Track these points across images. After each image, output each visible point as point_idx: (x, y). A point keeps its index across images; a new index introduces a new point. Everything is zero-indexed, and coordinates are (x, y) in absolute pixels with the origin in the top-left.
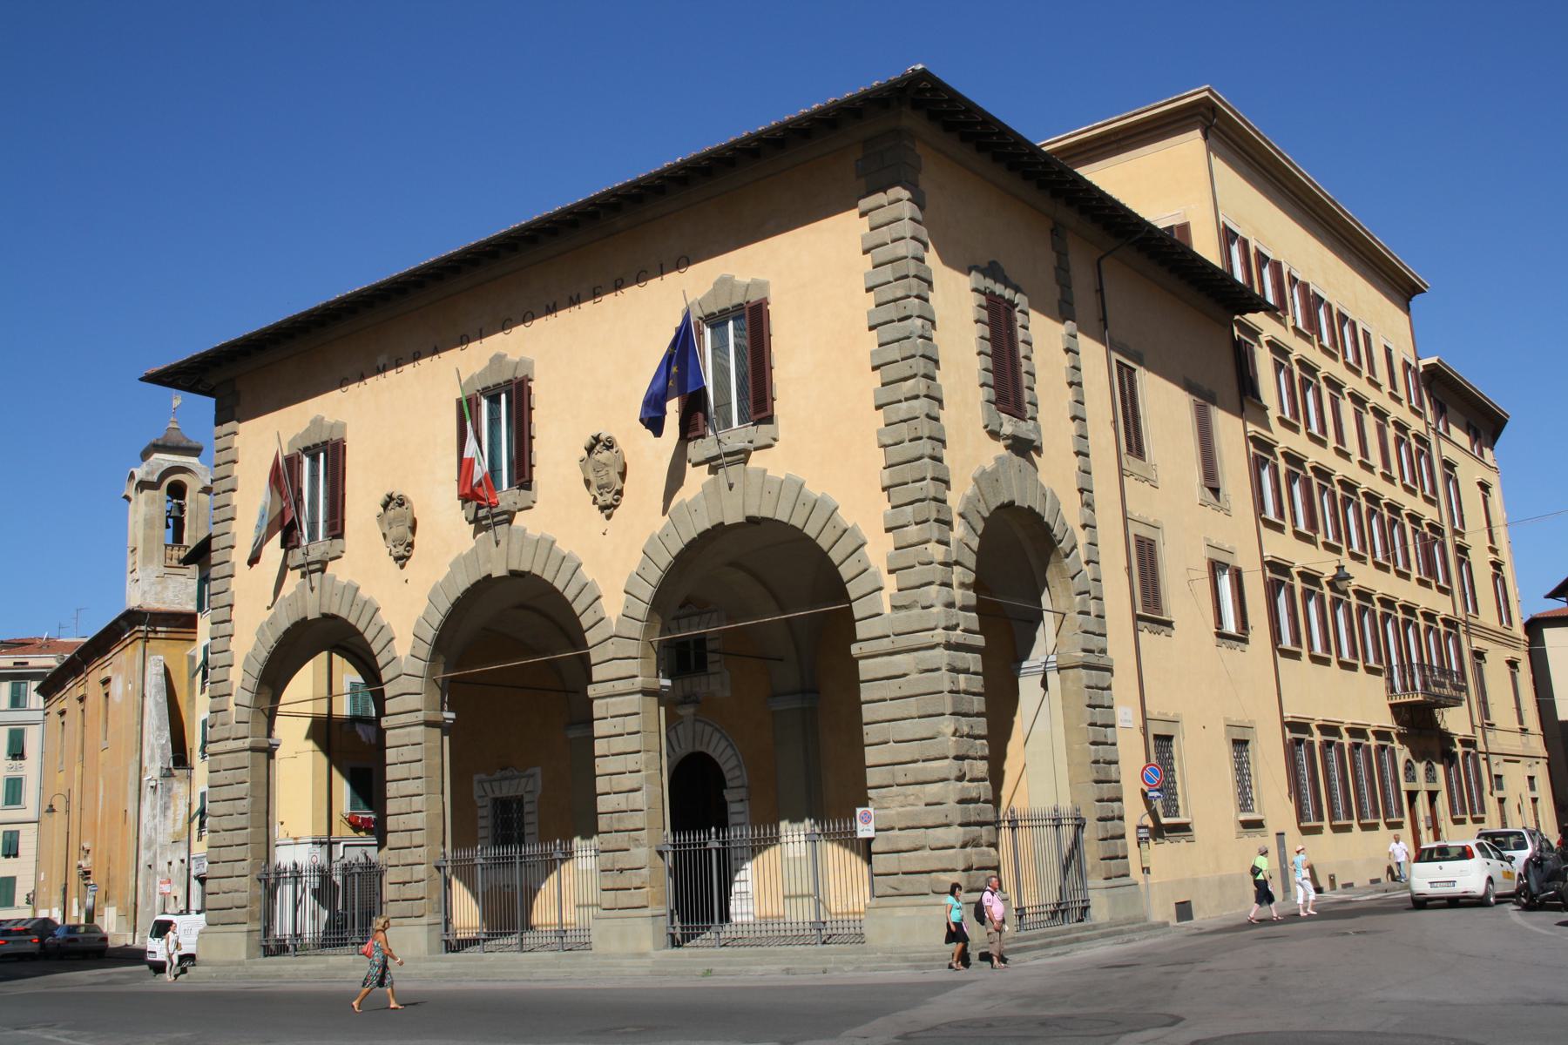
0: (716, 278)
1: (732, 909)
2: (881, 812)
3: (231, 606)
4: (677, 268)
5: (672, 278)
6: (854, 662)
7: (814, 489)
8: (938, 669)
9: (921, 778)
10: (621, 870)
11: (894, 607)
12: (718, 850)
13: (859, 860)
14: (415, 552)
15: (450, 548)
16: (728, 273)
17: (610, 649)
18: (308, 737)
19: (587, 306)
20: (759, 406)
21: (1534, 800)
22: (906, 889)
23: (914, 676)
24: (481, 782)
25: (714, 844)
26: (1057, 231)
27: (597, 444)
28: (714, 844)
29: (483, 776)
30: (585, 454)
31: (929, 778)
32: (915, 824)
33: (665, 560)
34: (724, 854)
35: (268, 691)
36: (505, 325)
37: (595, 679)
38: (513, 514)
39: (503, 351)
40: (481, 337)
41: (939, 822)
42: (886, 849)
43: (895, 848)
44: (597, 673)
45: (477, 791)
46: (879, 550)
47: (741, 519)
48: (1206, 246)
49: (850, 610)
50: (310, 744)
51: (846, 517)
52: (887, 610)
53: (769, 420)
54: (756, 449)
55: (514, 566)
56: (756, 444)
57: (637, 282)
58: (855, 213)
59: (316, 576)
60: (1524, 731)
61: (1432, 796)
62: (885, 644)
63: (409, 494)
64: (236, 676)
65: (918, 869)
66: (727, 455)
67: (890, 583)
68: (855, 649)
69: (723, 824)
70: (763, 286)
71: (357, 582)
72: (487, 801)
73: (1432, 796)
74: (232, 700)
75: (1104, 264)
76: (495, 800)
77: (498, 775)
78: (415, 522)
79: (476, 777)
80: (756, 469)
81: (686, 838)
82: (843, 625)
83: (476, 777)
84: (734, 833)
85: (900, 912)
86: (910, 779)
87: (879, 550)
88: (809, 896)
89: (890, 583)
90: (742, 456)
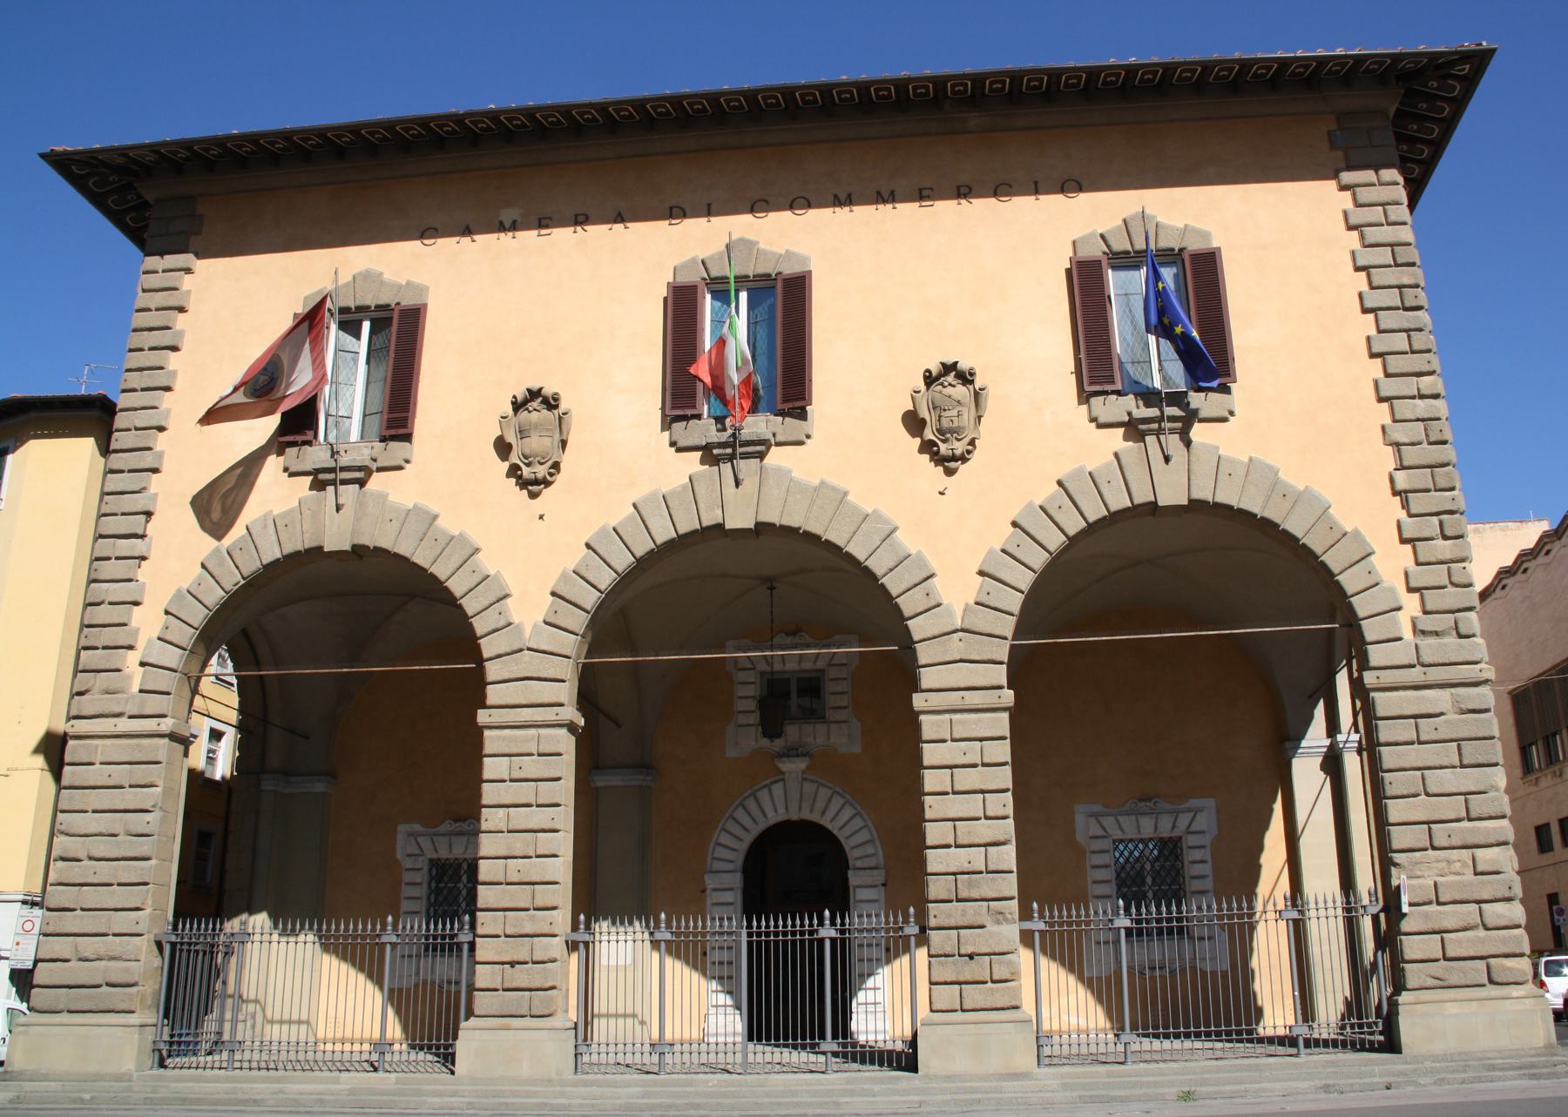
1: (854, 1026)
2: (1414, 882)
3: (149, 514)
4: (1062, 190)
5: (1052, 203)
6: (479, 731)
8: (1487, 710)
9: (1471, 840)
10: (971, 957)
12: (833, 940)
13: (362, 977)
14: (560, 480)
16: (377, 267)
18: (37, 751)
19: (907, 209)
22: (1454, 979)
23: (1452, 716)
24: (410, 834)
25: (827, 932)
27: (535, 398)
28: (827, 932)
29: (417, 827)
30: (509, 410)
31: (1482, 841)
32: (1465, 897)
33: (1295, 526)
34: (841, 947)
35: (201, 650)
36: (757, 205)
37: (489, 701)
38: (368, 471)
40: (1036, 192)
41: (1499, 895)
42: (1423, 928)
43: (1437, 927)
44: (494, 694)
45: (1084, 825)
47: (347, 547)
49: (480, 670)
50: (40, 761)
53: (801, 414)
54: (380, 470)
55: (766, 517)
56: (380, 464)
57: (995, 194)
58: (1331, 185)
59: (349, 493)
62: (953, 699)
64: (147, 623)
65: (1472, 954)
66: (343, 469)
67: (1411, 604)
68: (483, 716)
69: (840, 903)
70: (423, 290)
71: (434, 507)
72: (422, 863)
74: (133, 658)
76: (433, 863)
77: (447, 826)
79: (403, 828)
80: (778, 470)
81: (777, 926)
82: (473, 688)
83: (403, 828)
84: (854, 921)
85: (1452, 1009)
86: (1455, 841)
88: (599, 1016)
90: (760, 446)
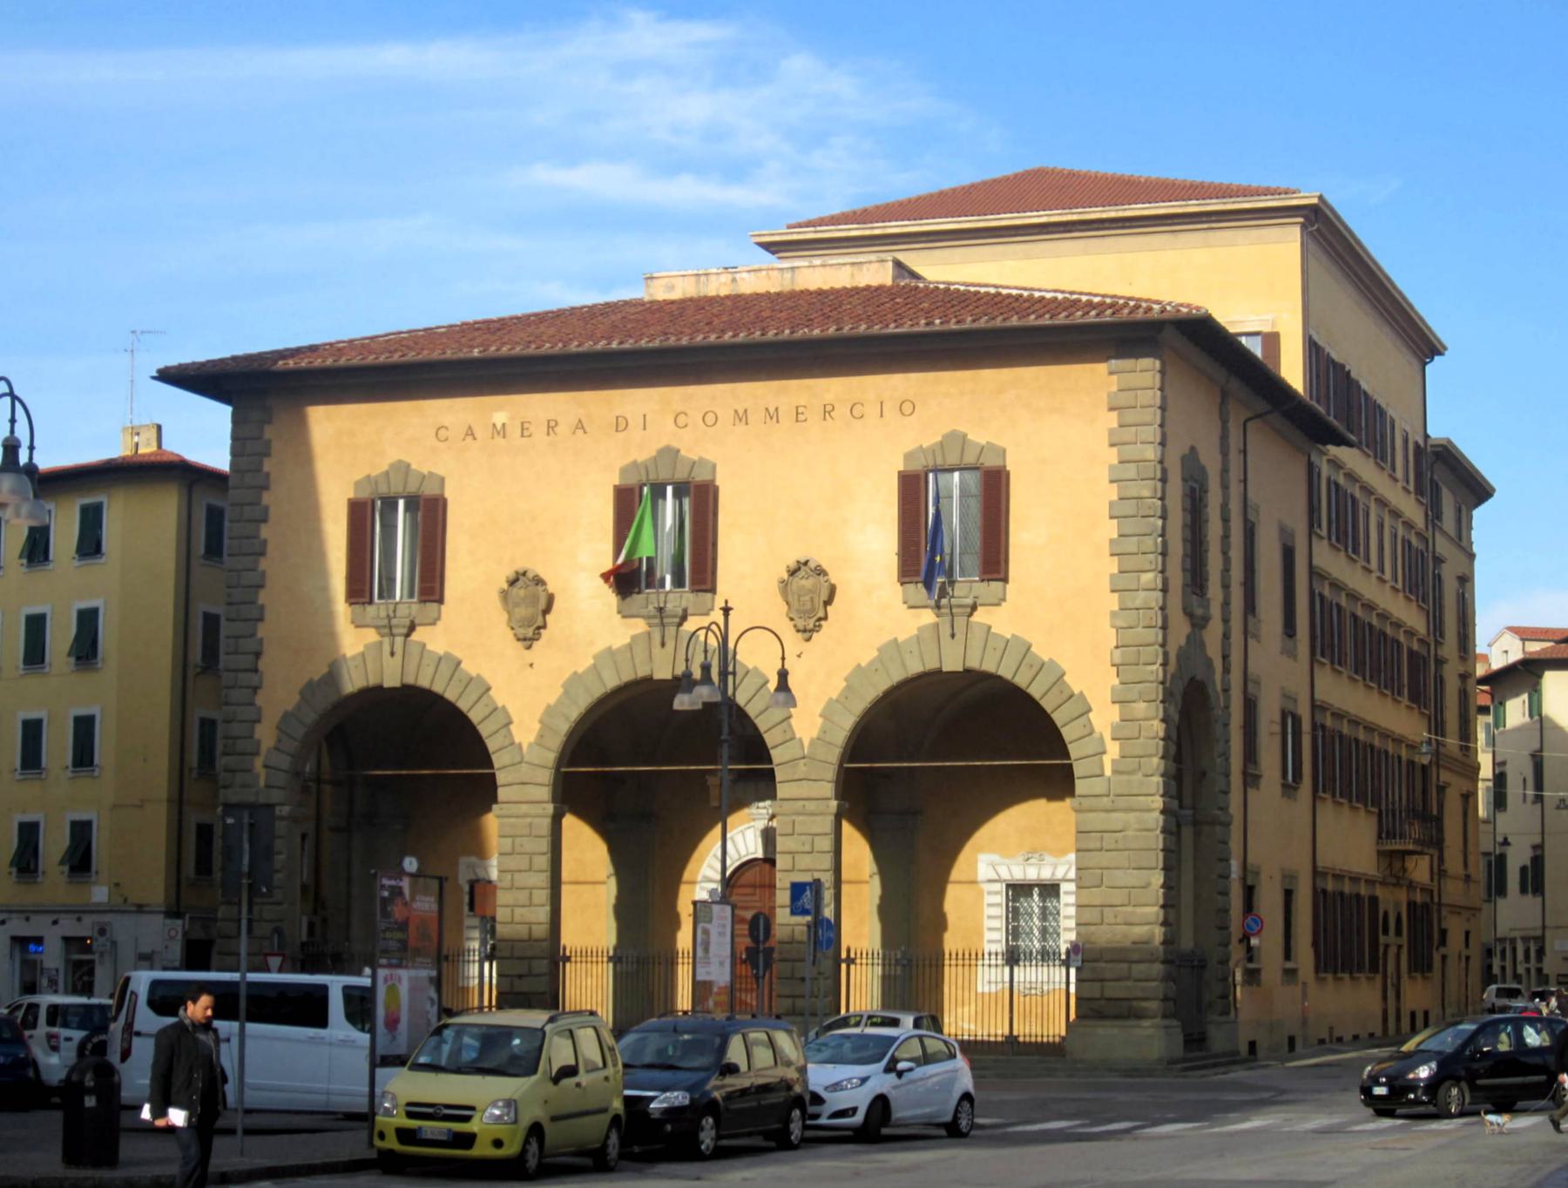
0: (946, 430)
7: (1042, 651)
11: (1115, 772)
15: (596, 638)
17: (802, 769)
20: (994, 564)
21: (1468, 958)
26: (1224, 396)
39: (675, 445)
46: (1104, 717)
48: (1293, 371)
51: (1075, 683)
52: (1108, 772)
60: (1467, 878)
61: (1400, 947)
63: (520, 565)
71: (458, 654)
73: (1400, 947)
75: (1249, 424)
78: (551, 599)
85: (1100, 1031)
87: (1104, 717)
89: (1113, 750)
